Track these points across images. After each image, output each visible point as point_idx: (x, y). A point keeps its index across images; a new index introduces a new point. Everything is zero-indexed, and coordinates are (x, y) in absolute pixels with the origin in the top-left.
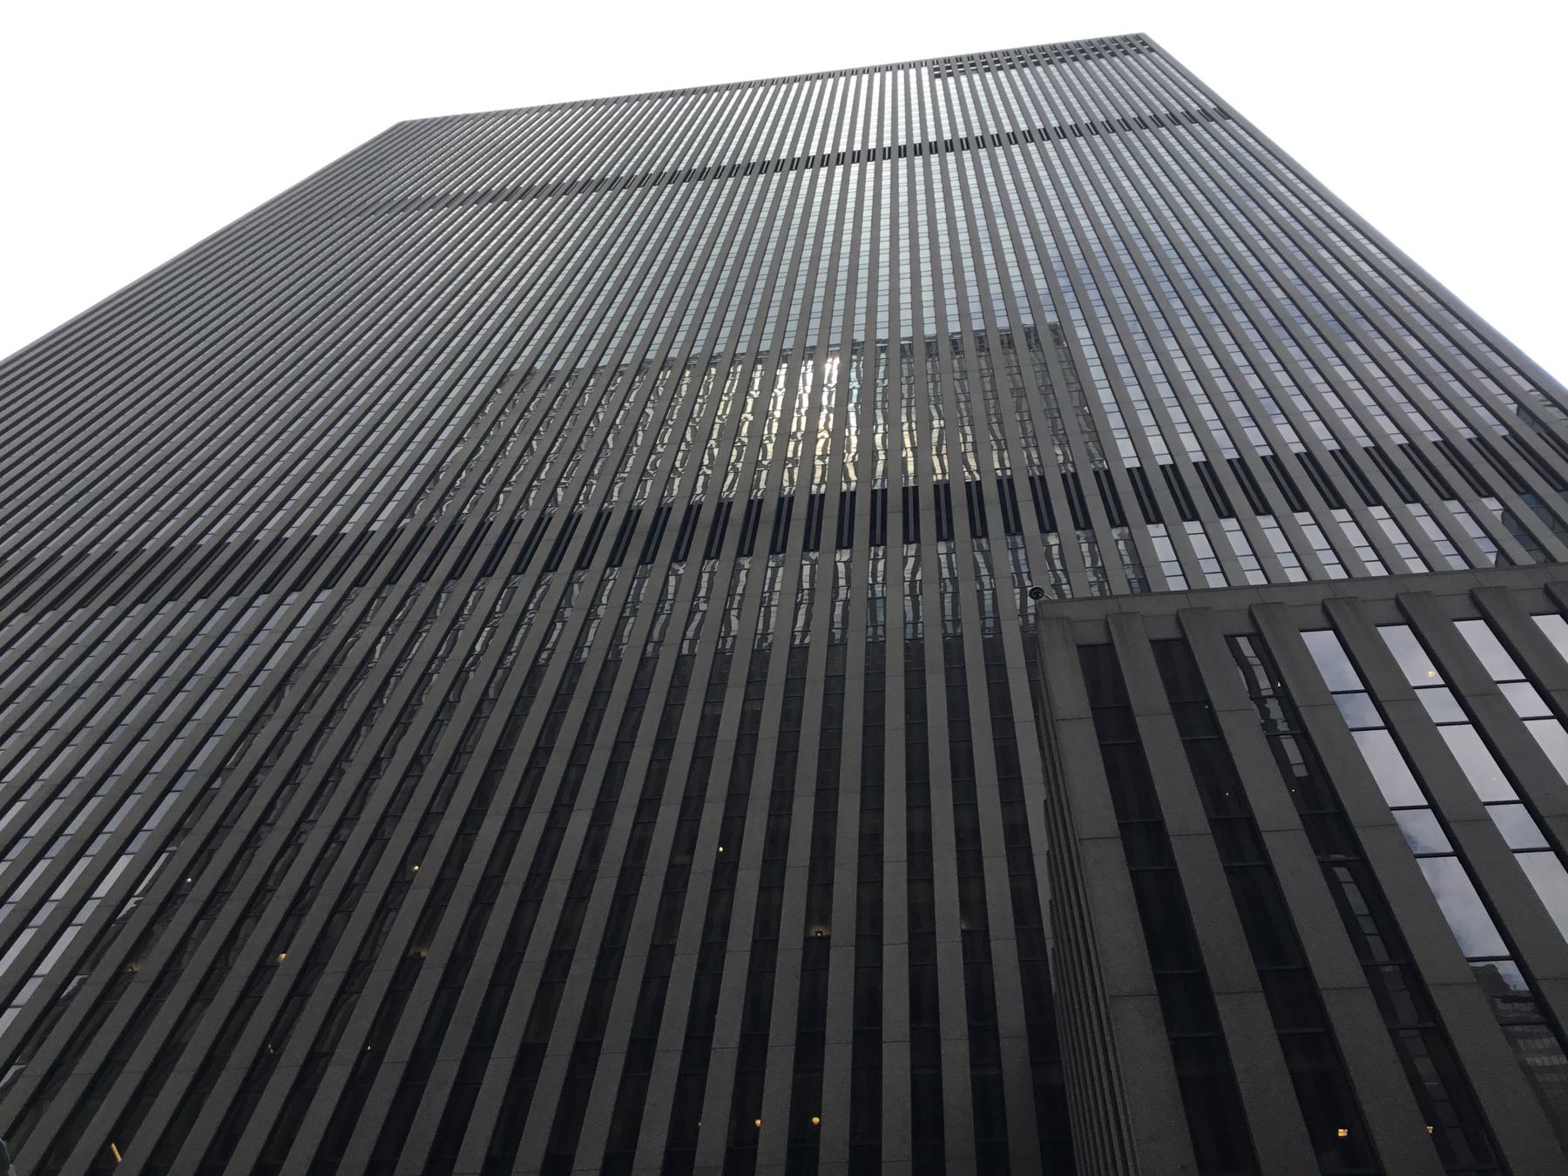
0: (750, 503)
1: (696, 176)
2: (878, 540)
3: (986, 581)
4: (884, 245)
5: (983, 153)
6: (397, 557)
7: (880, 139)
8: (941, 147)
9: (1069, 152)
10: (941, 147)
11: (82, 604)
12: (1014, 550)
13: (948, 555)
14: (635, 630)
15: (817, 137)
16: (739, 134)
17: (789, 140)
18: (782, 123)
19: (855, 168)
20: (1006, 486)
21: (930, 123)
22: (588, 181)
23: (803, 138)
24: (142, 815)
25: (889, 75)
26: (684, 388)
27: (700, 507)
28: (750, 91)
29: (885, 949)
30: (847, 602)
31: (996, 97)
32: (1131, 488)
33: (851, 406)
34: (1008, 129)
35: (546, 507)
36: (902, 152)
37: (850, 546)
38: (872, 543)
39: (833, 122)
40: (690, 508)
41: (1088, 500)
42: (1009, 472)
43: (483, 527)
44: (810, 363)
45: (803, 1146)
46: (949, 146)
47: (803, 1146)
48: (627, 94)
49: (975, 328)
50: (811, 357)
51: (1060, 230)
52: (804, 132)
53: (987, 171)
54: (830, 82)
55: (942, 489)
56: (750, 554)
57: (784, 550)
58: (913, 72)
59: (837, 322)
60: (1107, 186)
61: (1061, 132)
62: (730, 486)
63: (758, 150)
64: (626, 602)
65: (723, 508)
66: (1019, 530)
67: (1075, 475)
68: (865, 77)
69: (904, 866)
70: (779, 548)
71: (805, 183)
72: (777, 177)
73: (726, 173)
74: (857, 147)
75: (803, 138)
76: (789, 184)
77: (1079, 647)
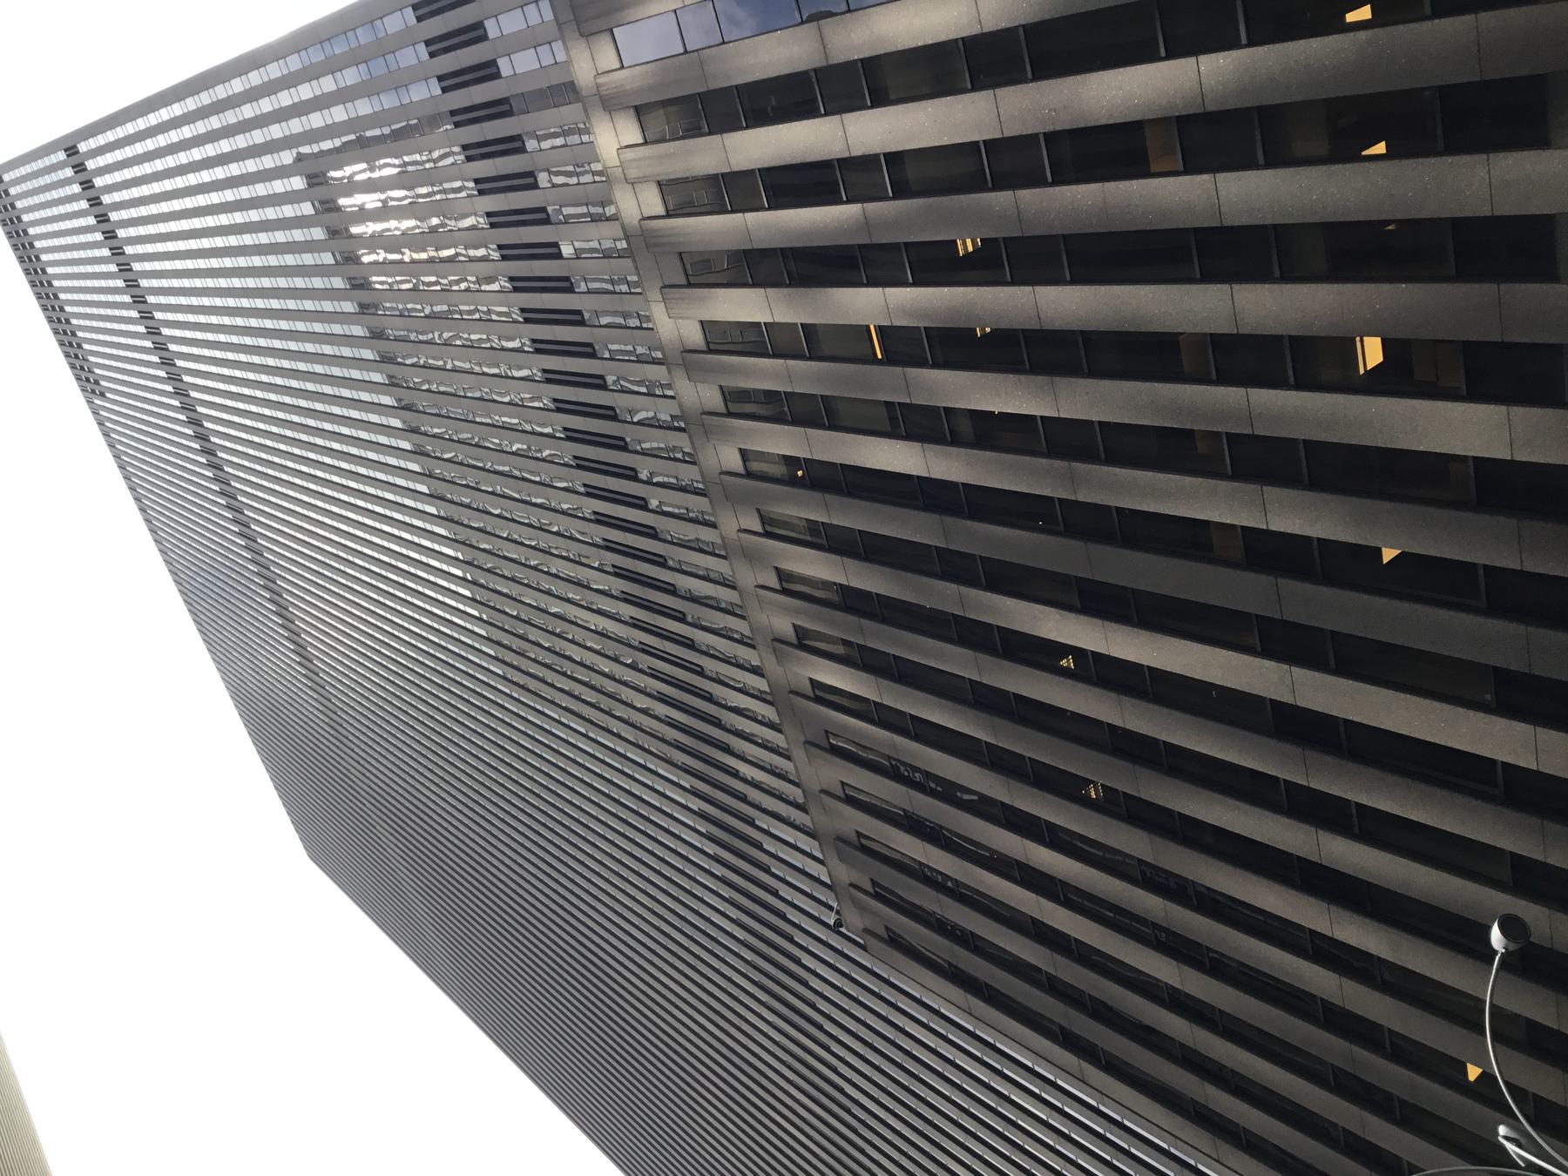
1: (172, 369)
6: (567, 359)
7: (66, 182)
11: (760, 847)
13: (539, 139)
15: (130, 341)
20: (496, 220)
22: (222, 493)
23: (123, 327)
26: (436, 430)
31: (75, 269)
32: (513, 230)
35: (584, 519)
37: (531, 174)
38: (535, 186)
39: (41, 181)
42: (456, 149)
43: (609, 546)
48: (107, 449)
52: (89, 269)
55: (446, 83)
56: (556, 245)
57: (567, 279)
59: (318, 283)
64: (670, 459)
65: (496, 220)
70: (566, 284)
75: (123, 327)
77: (659, 184)
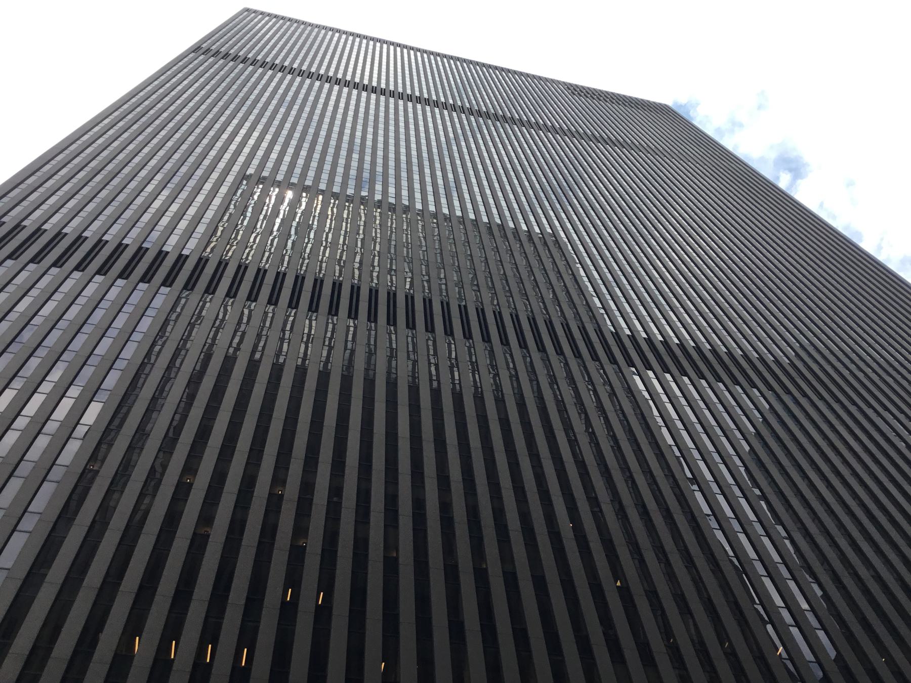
0: (278, 273)
2: (333, 313)
3: (287, 333)
4: (335, 136)
5: (392, 100)
6: (63, 250)
8: (361, 87)
9: (438, 116)
10: (361, 87)
12: (390, 334)
14: (223, 338)
16: (281, 43)
17: (283, 54)
18: (436, 72)
19: (308, 81)
21: (350, 70)
24: (743, 521)
25: (344, 36)
27: (207, 260)
28: (267, 18)
29: (275, 551)
30: (244, 333)
33: (362, 236)
34: (409, 92)
36: (338, 82)
38: (290, 306)
40: (200, 259)
41: (472, 323)
44: (261, 186)
45: (122, 659)
46: (365, 88)
47: (122, 659)
49: (334, 190)
50: (262, 183)
51: (411, 155)
53: (430, 119)
54: (323, 32)
58: (365, 41)
60: (493, 150)
61: (419, 100)
62: (249, 256)
63: (263, 53)
65: (161, 255)
66: (376, 321)
67: (465, 307)
68: (323, 32)
69: (234, 497)
71: (286, 82)
72: (260, 70)
73: (201, 51)
74: (304, 68)
76: (266, 77)
